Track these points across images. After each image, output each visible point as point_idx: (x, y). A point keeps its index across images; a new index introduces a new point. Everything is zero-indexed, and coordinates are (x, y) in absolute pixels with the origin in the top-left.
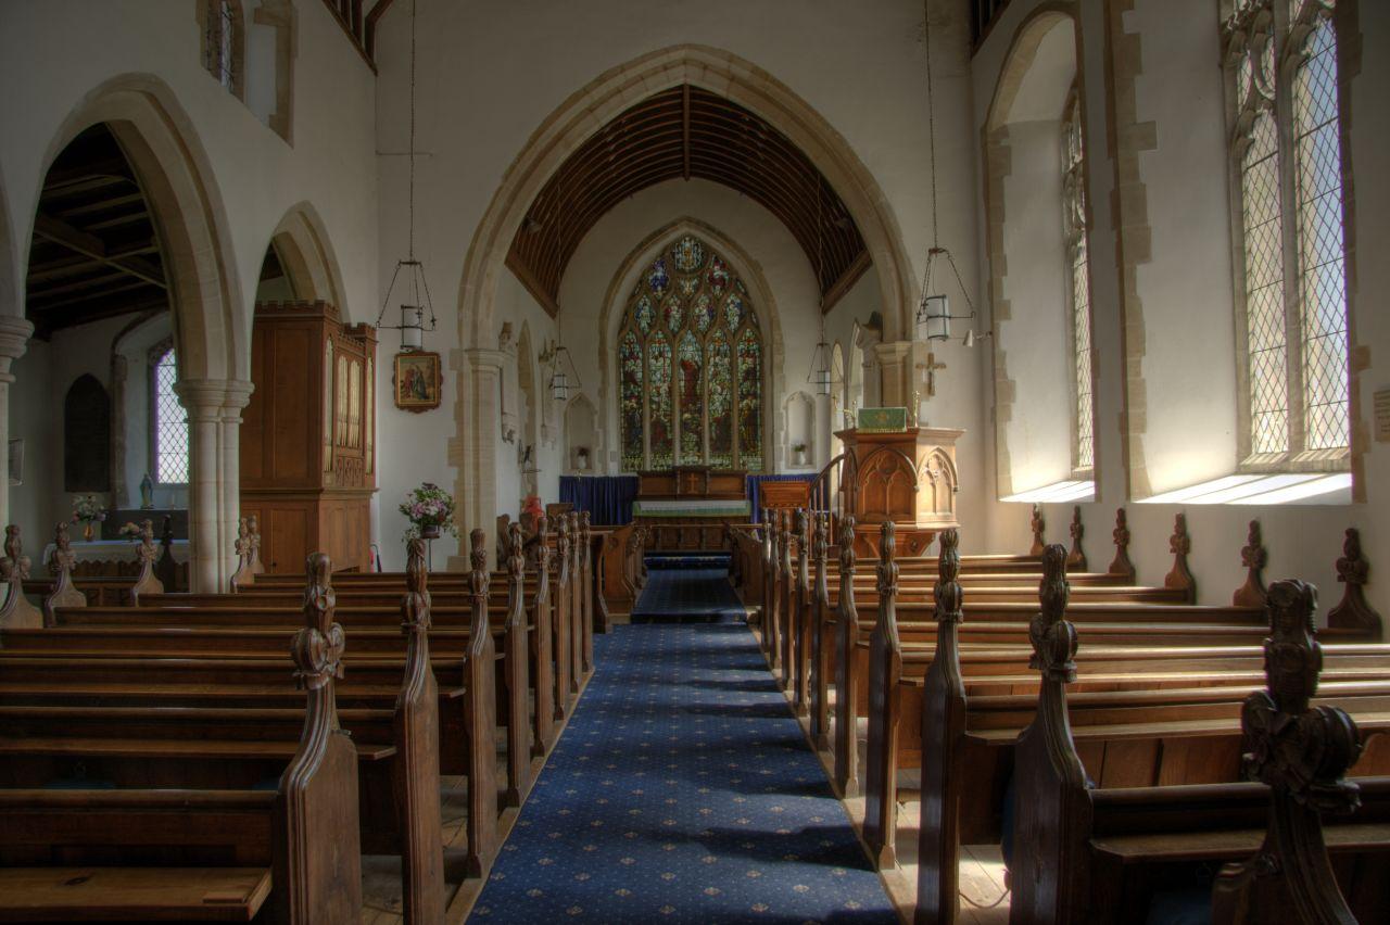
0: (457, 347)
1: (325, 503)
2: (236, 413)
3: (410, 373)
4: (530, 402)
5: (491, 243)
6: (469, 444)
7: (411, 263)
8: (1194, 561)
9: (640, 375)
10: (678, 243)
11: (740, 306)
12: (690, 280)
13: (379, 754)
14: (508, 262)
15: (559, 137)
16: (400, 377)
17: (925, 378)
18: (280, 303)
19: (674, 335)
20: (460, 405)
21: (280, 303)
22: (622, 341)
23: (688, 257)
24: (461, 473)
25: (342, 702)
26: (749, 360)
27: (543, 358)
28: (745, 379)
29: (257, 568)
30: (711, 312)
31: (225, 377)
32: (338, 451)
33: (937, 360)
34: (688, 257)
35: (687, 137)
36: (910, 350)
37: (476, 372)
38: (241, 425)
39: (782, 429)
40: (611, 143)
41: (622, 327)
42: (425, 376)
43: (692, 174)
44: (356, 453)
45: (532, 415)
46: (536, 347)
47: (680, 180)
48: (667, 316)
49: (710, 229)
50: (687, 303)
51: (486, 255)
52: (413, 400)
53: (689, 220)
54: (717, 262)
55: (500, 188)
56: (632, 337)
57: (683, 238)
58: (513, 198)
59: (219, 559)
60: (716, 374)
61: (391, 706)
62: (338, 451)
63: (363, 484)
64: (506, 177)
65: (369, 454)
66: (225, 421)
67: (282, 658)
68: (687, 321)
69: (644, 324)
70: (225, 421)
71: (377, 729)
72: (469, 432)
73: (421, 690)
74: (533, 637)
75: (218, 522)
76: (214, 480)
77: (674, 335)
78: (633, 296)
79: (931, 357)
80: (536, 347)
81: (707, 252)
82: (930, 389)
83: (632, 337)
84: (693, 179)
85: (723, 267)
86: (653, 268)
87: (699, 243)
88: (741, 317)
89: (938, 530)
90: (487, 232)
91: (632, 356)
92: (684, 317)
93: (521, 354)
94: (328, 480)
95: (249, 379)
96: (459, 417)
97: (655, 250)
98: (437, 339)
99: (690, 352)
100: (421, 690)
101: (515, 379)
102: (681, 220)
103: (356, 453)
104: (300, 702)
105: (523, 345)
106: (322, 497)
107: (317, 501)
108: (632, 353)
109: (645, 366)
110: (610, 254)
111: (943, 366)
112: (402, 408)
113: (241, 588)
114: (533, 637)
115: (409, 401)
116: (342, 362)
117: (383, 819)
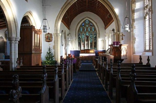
0: (54, 33)
1: (32, 55)
2: (17, 42)
3: (48, 36)
4: (66, 41)
5: (59, 18)
6: (56, 47)
7: (45, 19)
8: (150, 62)
9: (81, 37)
10: (86, 20)
11: (94, 28)
12: (87, 25)
13: (51, 87)
14: (62, 21)
15: (69, 3)
16: (46, 37)
17: (122, 37)
18: (28, 25)
19: (85, 32)
20: (55, 41)
21: (28, 25)
22: (78, 33)
23: (87, 22)
24: (55, 50)
25: (58, 74)
26: (95, 35)
27: (68, 35)
28: (95, 38)
29: (21, 64)
30: (90, 29)
31: (15, 36)
32: (36, 47)
33: (124, 35)
34: (87, 22)
35: (87, 6)
36: (120, 33)
37: (57, 36)
38: (18, 44)
39: (121, 26)
40: (77, 6)
41: (78, 31)
42: (50, 37)
43: (88, 11)
44: (38, 48)
45: (66, 42)
46: (67, 34)
47: (86, 12)
48: (84, 30)
49: (90, 18)
50: (87, 28)
51: (59, 20)
52: (48, 40)
53: (87, 17)
54: (91, 23)
55: (60, 10)
56: (80, 33)
57: (86, 19)
58: (62, 12)
59: (14, 64)
60: (91, 37)
61: (53, 81)
62: (36, 47)
63: (40, 52)
64: (61, 9)
65: (41, 48)
66: (16, 43)
67: (54, 70)
68: (87, 30)
69: (81, 31)
70: (16, 43)
71: (51, 84)
72: (56, 44)
73: (57, 78)
74: (65, 75)
75: (14, 58)
76: (14, 52)
77: (85, 32)
78: (80, 27)
79: (123, 34)
80: (67, 34)
81: (90, 21)
82: (122, 39)
83: (80, 33)
84: (88, 12)
85: (92, 23)
86: (82, 24)
87: (88, 20)
88: (94, 30)
89: (11, 60)
90: (58, 17)
91: (80, 35)
92: (86, 30)
93: (65, 34)
94: (33, 52)
95: (19, 37)
96: (55, 43)
97: (83, 21)
98: (50, 31)
99: (87, 34)
100: (57, 78)
101: (64, 38)
102: (86, 17)
103: (38, 48)
104: (54, 74)
105: (65, 33)
106: (32, 54)
107: (32, 55)
108: (80, 35)
109: (81, 36)
110: (77, 21)
111: (125, 36)
112: (46, 41)
113: (17, 69)
114: (65, 75)
115: (47, 40)
116: (36, 35)
117: (52, 93)
